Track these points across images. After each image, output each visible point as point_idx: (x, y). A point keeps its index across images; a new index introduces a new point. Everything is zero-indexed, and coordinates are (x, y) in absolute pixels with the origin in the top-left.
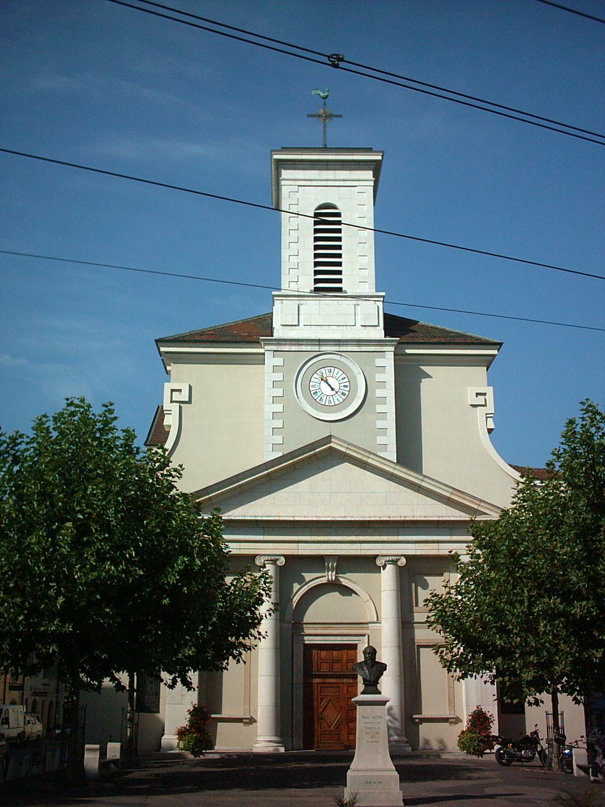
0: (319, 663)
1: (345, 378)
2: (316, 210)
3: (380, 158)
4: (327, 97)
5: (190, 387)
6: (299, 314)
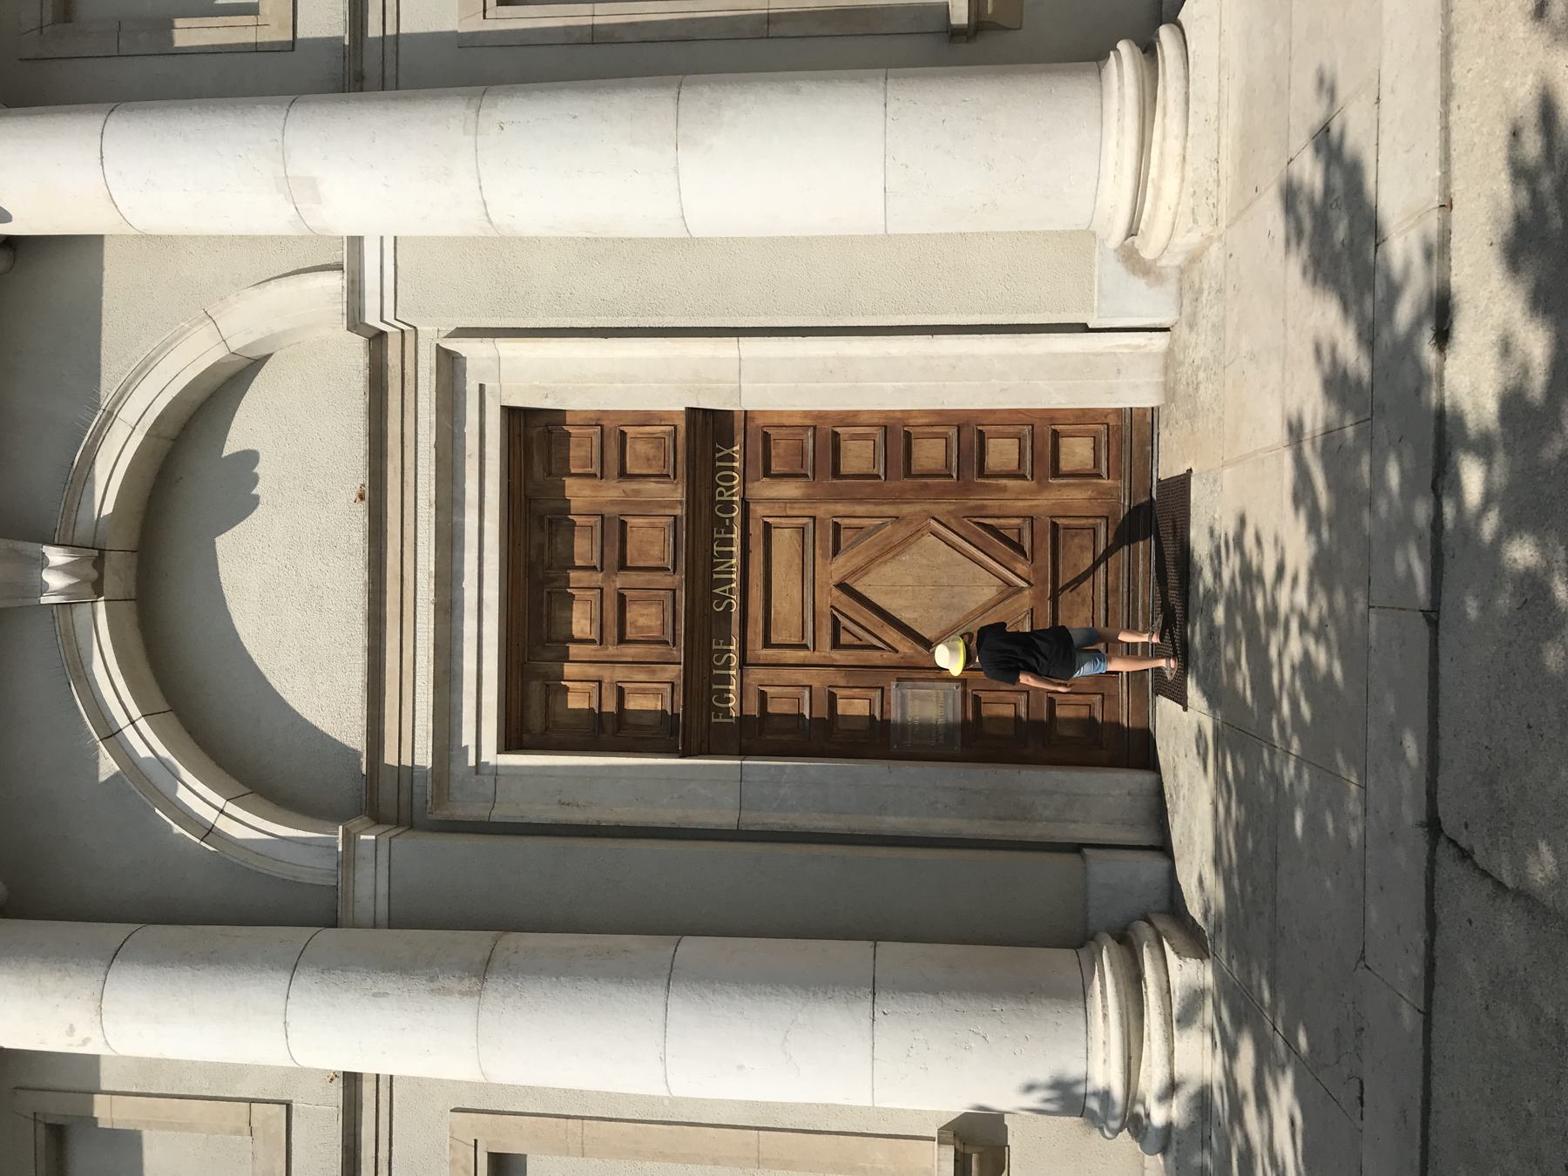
0: (840, 657)
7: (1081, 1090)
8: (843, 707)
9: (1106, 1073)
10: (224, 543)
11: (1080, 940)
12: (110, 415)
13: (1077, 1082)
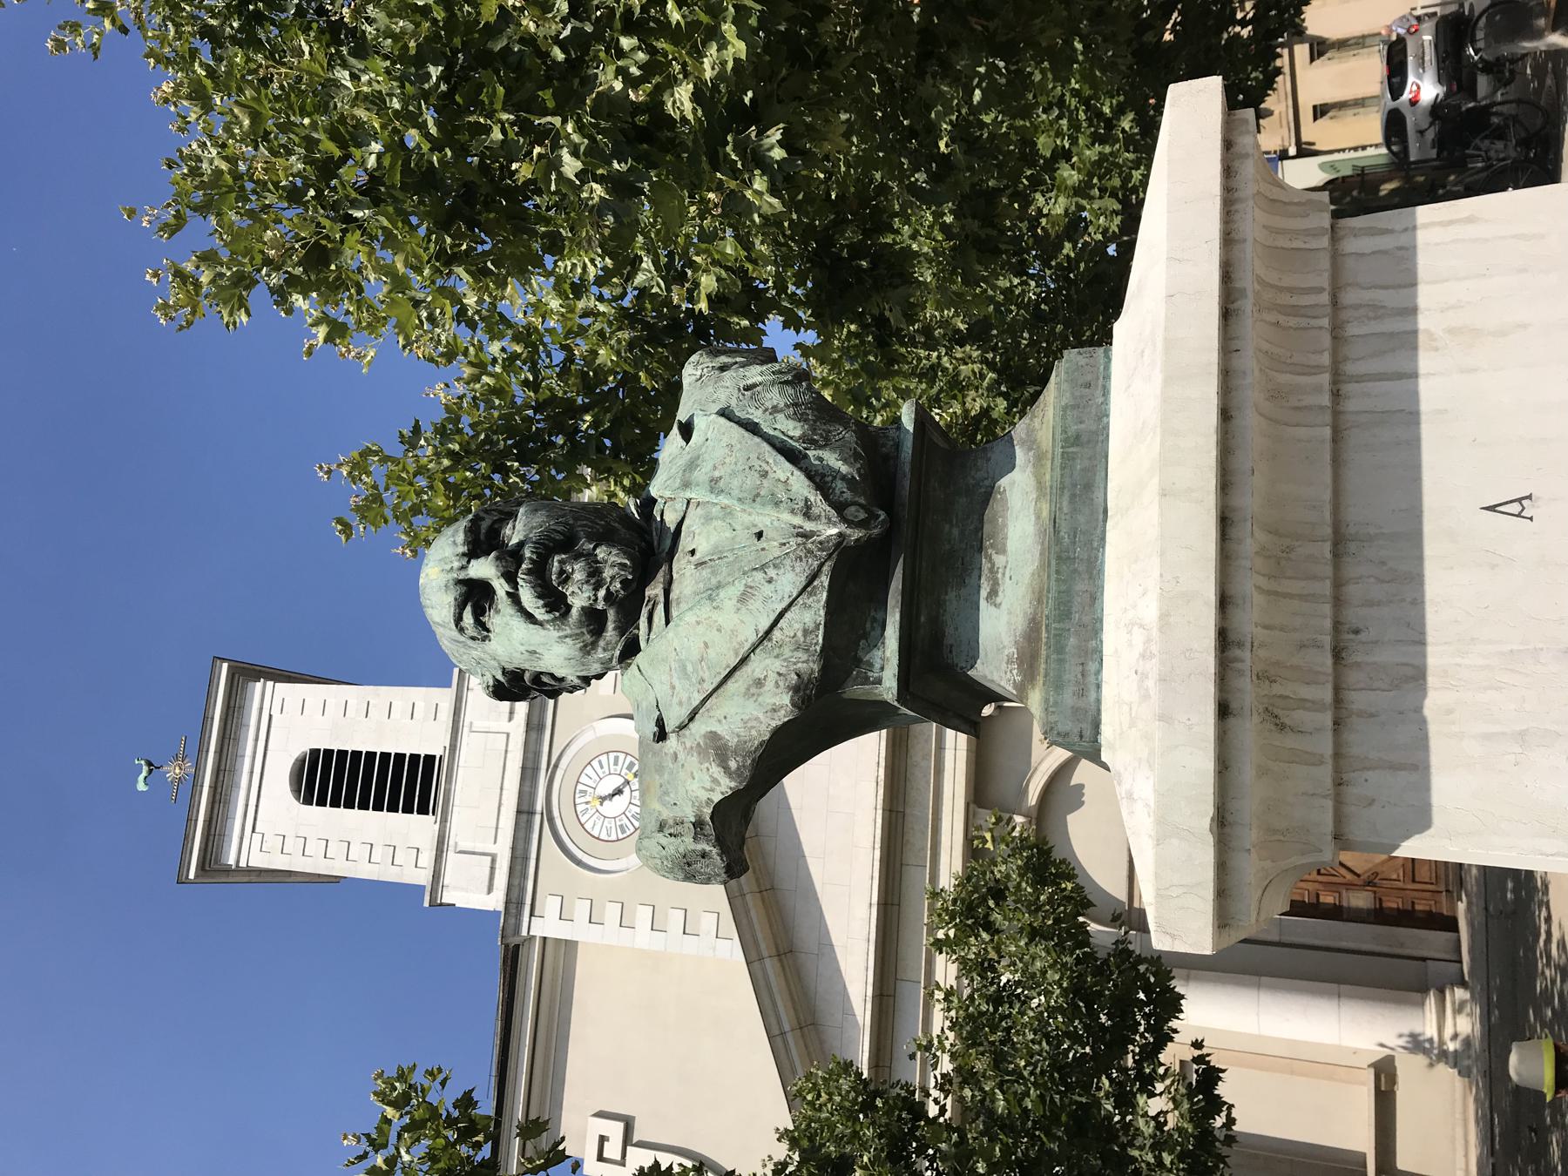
0: (1320, 878)
1: (600, 762)
2: (298, 799)
3: (225, 665)
4: (149, 764)
5: (601, 1114)
6: (474, 853)
7: (1421, 1038)
8: (1322, 899)
9: (1430, 1031)
10: (1070, 818)
11: (1423, 990)
12: (1036, 769)
13: (1419, 1035)
